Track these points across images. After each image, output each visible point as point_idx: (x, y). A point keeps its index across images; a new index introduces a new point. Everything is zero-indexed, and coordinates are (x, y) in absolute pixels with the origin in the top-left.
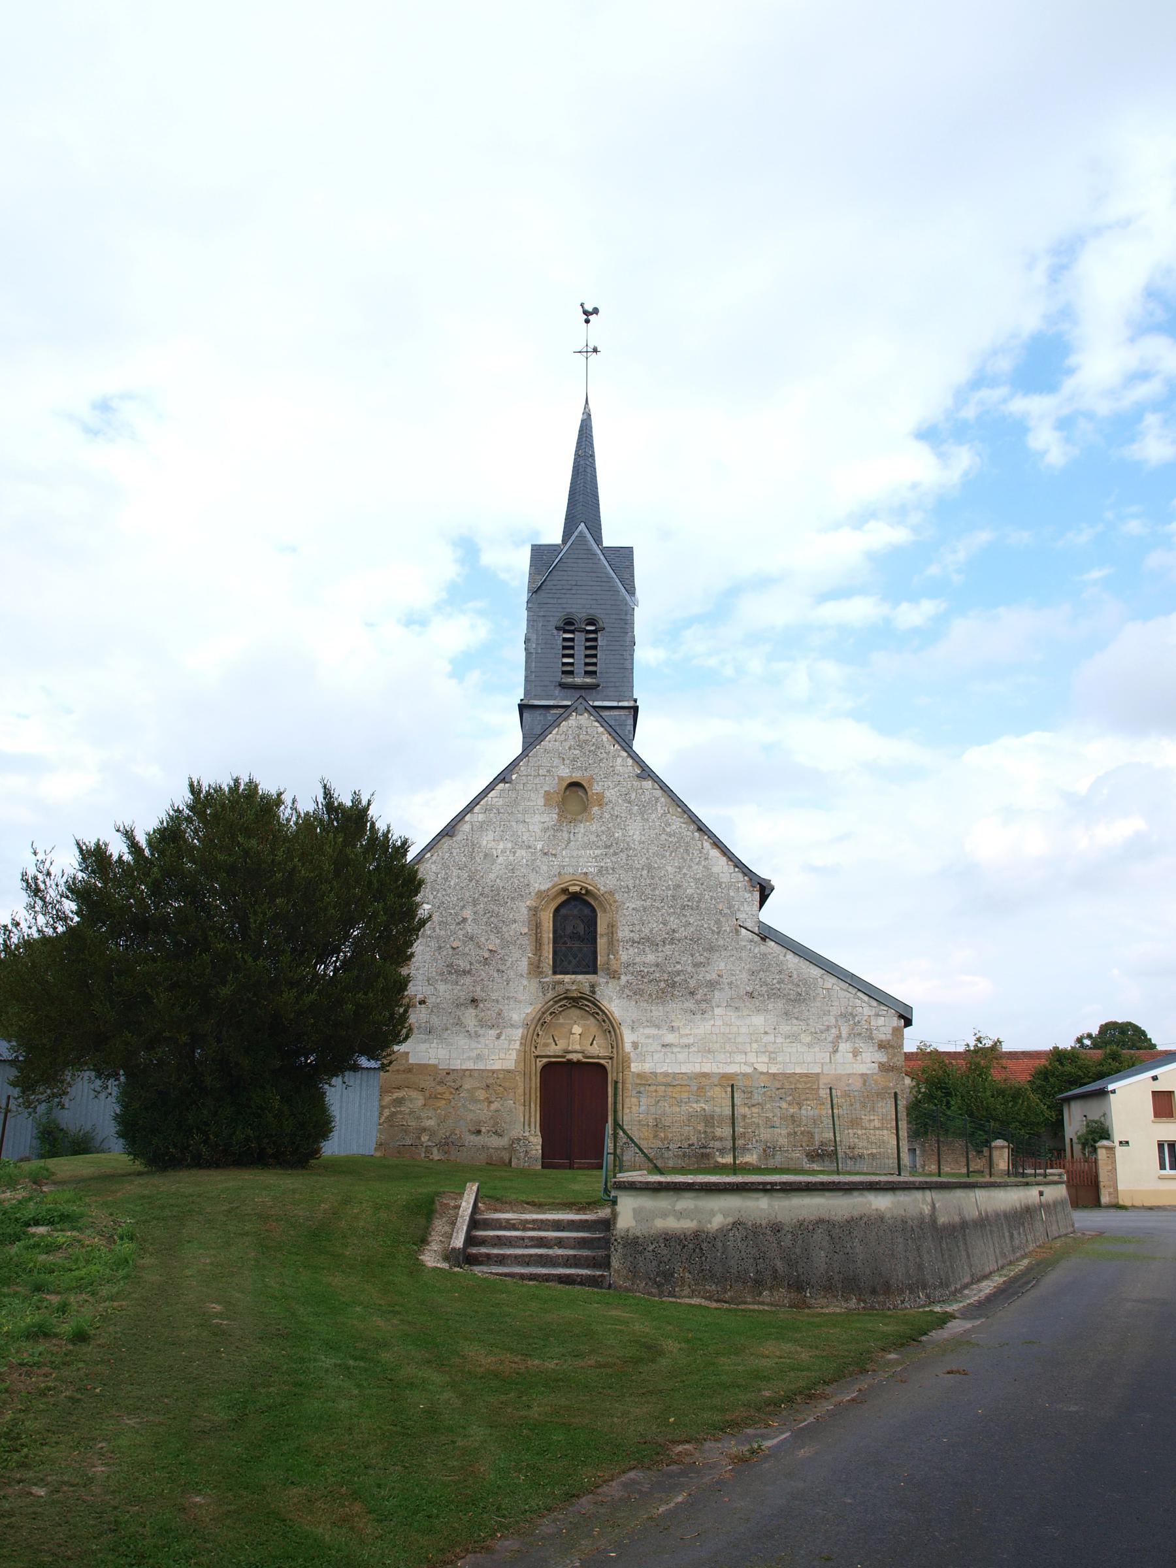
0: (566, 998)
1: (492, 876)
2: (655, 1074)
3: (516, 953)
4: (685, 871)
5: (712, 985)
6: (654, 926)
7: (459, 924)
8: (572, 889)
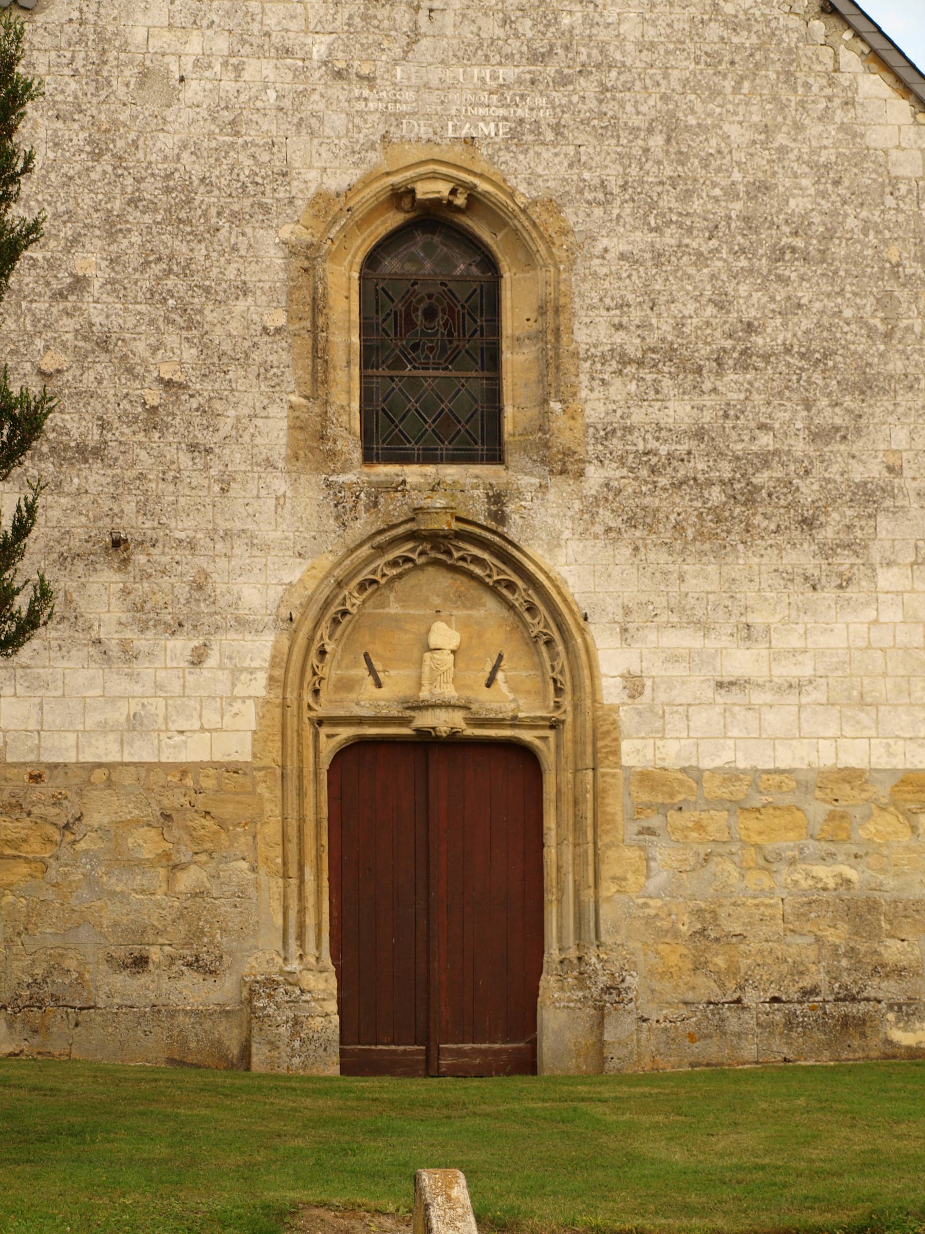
0: (412, 536)
1: (167, 142)
2: (695, 774)
3: (249, 393)
4: (781, 139)
5: (869, 498)
6: (685, 310)
7: (60, 295)
8: (426, 190)
